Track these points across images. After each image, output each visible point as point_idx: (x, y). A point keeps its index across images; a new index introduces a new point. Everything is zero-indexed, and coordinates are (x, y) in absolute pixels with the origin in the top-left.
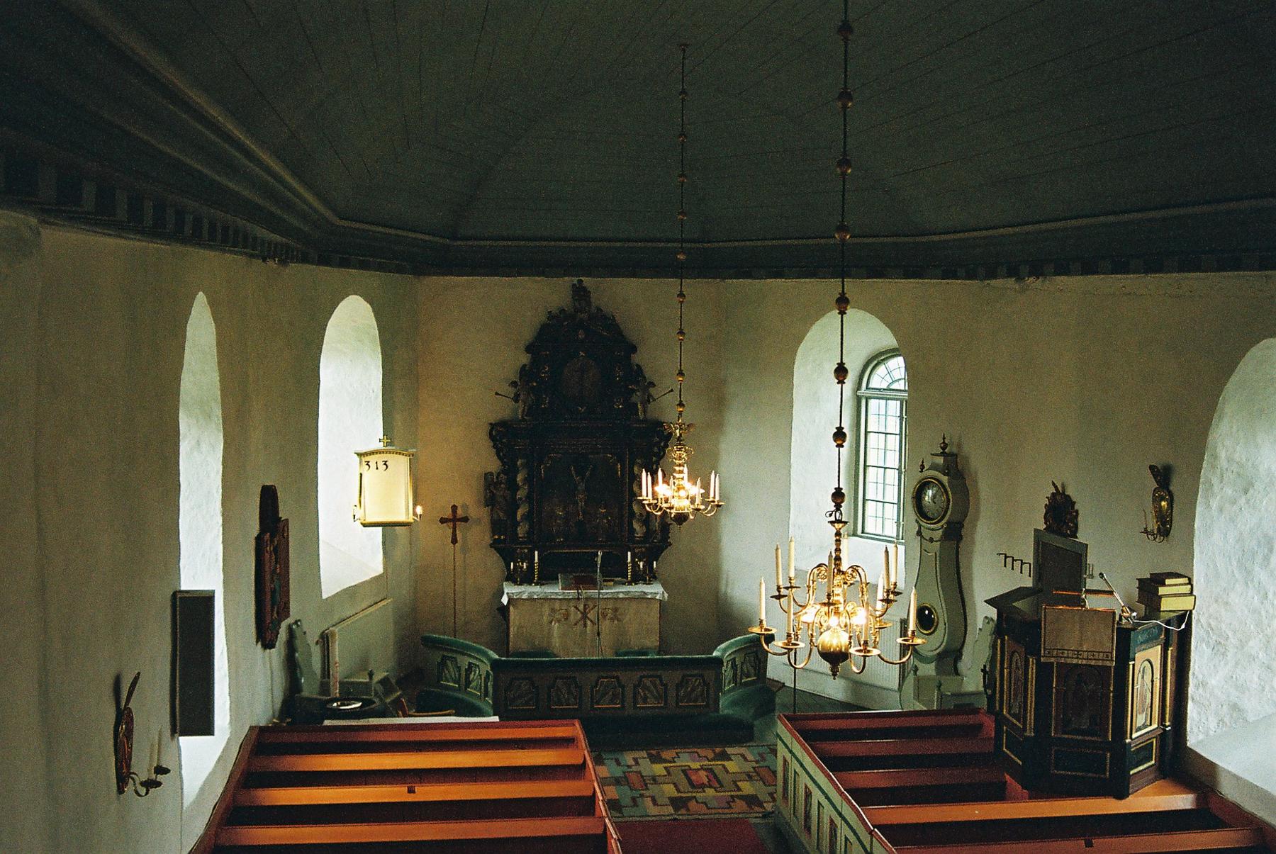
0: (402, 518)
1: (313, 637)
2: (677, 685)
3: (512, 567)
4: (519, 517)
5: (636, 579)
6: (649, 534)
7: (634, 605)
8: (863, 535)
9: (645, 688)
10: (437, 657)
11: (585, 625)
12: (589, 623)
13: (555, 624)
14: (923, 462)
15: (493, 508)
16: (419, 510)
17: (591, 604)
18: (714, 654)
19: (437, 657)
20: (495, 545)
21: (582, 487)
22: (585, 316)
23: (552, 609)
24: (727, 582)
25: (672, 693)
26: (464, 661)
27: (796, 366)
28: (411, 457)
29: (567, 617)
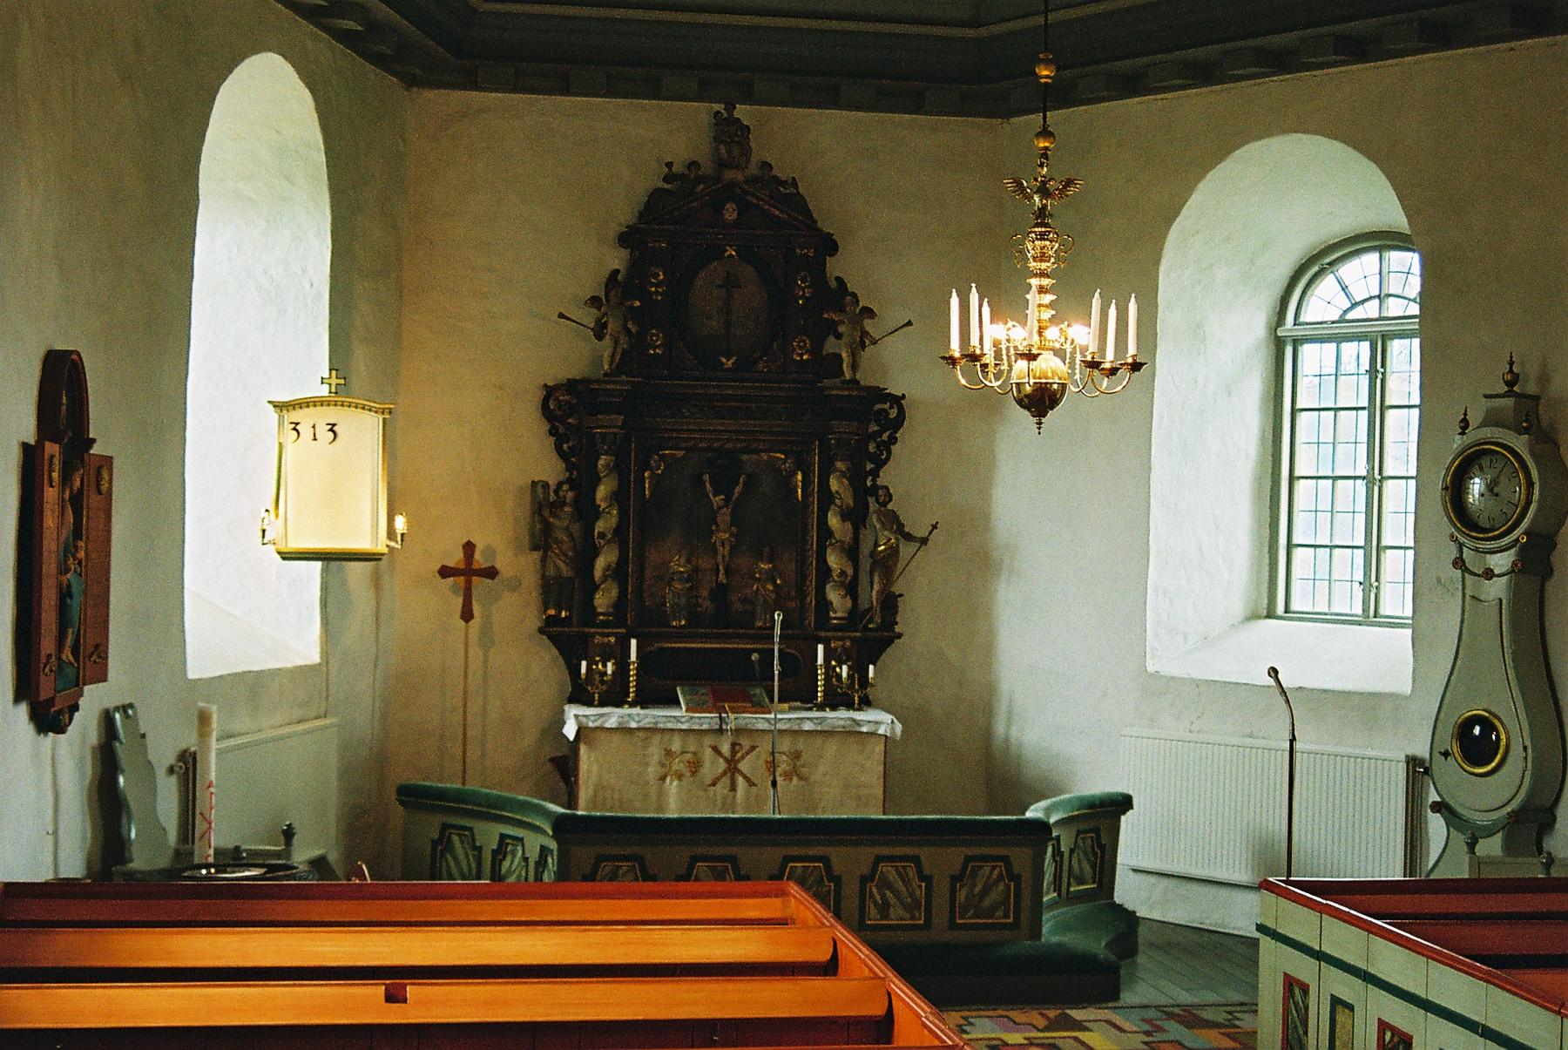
0: (363, 544)
1: (162, 753)
2: (954, 879)
3: (583, 670)
4: (598, 574)
5: (836, 700)
6: (855, 616)
7: (832, 747)
8: (1287, 615)
9: (886, 884)
10: (431, 826)
11: (733, 788)
12: (740, 780)
13: (672, 781)
14: (1465, 414)
15: (545, 553)
16: (400, 523)
17: (746, 743)
18: (1029, 814)
19: (431, 826)
20: (551, 630)
21: (724, 517)
22: (738, 176)
23: (666, 750)
24: (1010, 713)
25: (942, 888)
26: (489, 834)
27: (1162, 268)
28: (387, 416)
29: (695, 766)
